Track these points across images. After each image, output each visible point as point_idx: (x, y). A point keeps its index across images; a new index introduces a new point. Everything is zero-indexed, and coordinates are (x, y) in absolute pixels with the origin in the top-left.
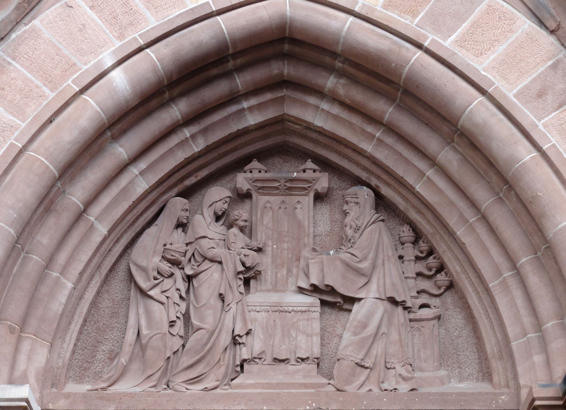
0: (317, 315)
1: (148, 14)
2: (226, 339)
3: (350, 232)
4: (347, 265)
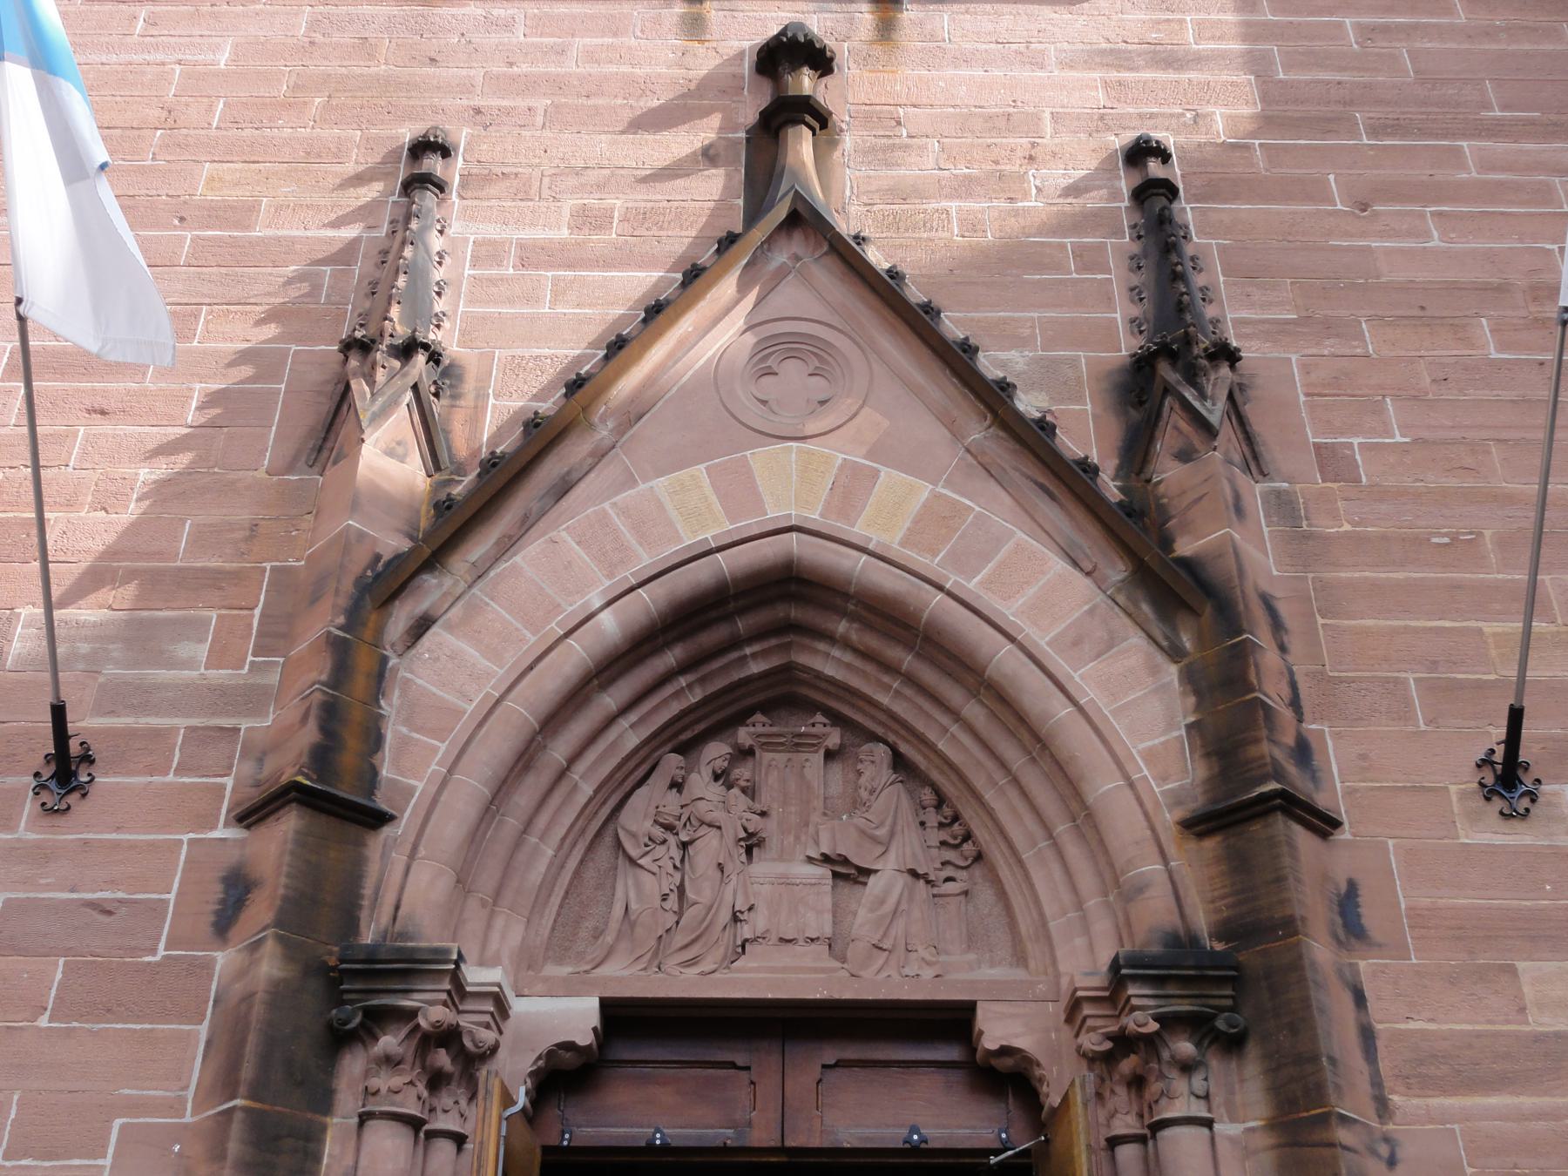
0: (829, 888)
1: (640, 550)
2: (725, 916)
3: (864, 794)
4: (863, 832)
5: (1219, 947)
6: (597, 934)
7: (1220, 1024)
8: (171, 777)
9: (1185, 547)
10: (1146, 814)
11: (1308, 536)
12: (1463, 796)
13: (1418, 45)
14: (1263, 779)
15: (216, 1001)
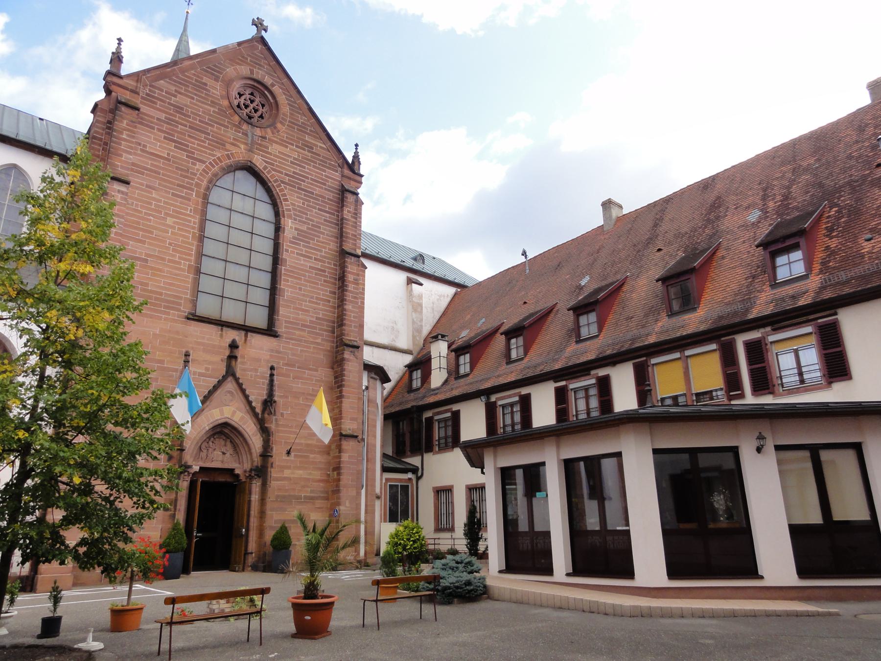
9: (266, 425)
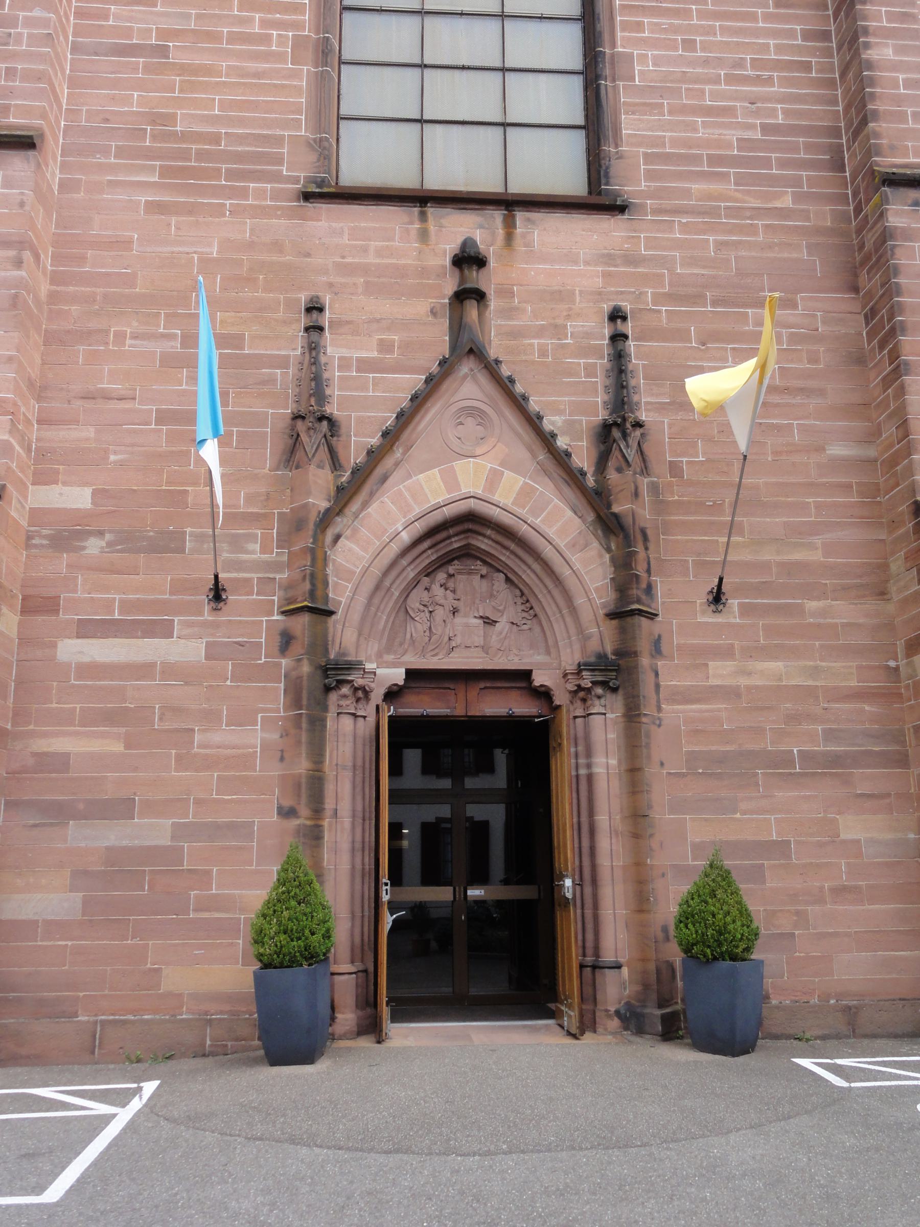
0: (482, 628)
1: (415, 506)
2: (446, 639)
3: (495, 593)
4: (494, 607)
5: (613, 657)
6: (401, 644)
7: (611, 684)
8: (255, 597)
9: (616, 509)
10: (593, 610)
11: (662, 501)
12: (701, 604)
13: (740, 254)
14: (633, 603)
15: (285, 677)
